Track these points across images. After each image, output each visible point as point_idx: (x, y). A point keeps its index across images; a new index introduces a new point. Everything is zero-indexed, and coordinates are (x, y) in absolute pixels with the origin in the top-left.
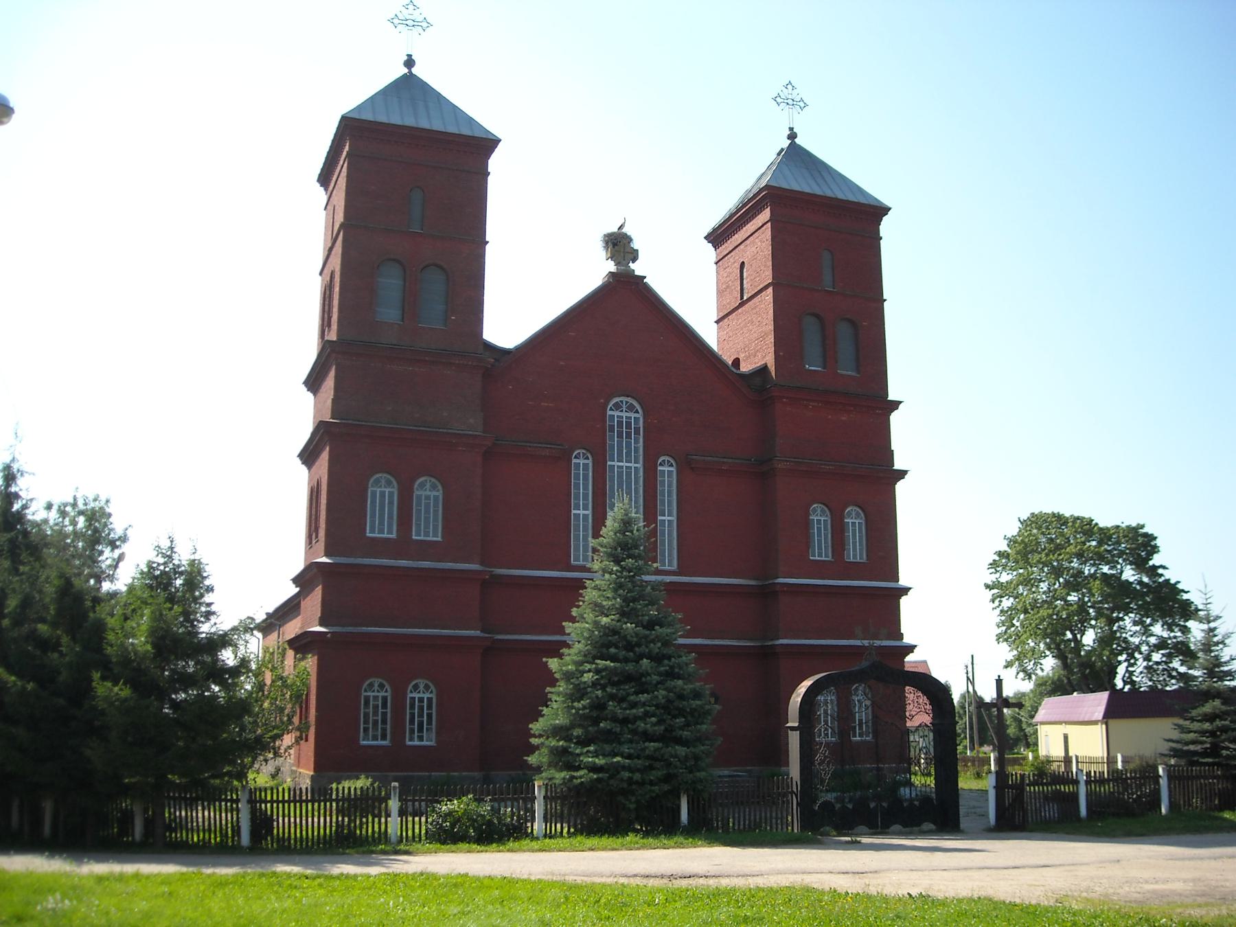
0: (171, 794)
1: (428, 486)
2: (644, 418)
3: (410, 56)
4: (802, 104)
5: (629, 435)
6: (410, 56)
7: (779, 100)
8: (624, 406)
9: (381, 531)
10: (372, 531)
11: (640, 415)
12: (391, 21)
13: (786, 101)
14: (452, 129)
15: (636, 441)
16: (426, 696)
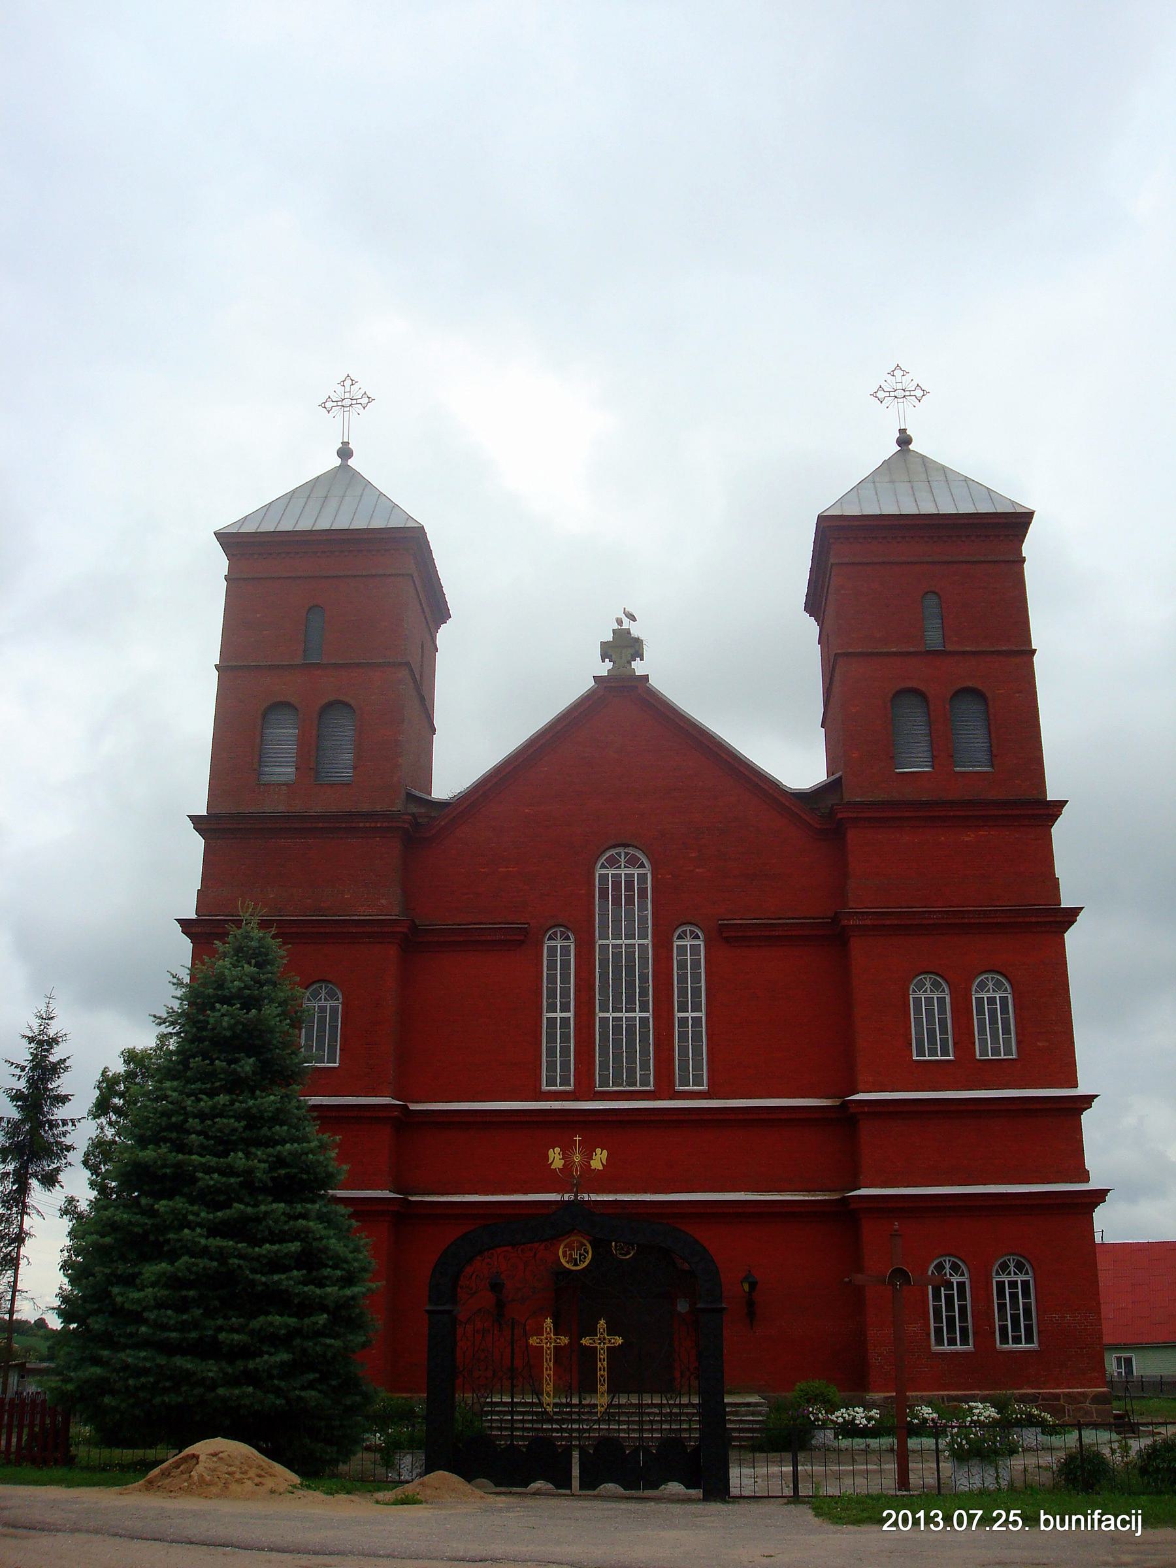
0: (1019, 1416)
1: (991, 985)
2: (652, 874)
3: (902, 431)
4: (919, 393)
5: (630, 901)
6: (902, 431)
7: (881, 394)
8: (623, 860)
9: (933, 1052)
10: (921, 1053)
11: (647, 871)
12: (925, 393)
13: (892, 394)
14: (966, 508)
15: (643, 908)
16: (1020, 1278)
